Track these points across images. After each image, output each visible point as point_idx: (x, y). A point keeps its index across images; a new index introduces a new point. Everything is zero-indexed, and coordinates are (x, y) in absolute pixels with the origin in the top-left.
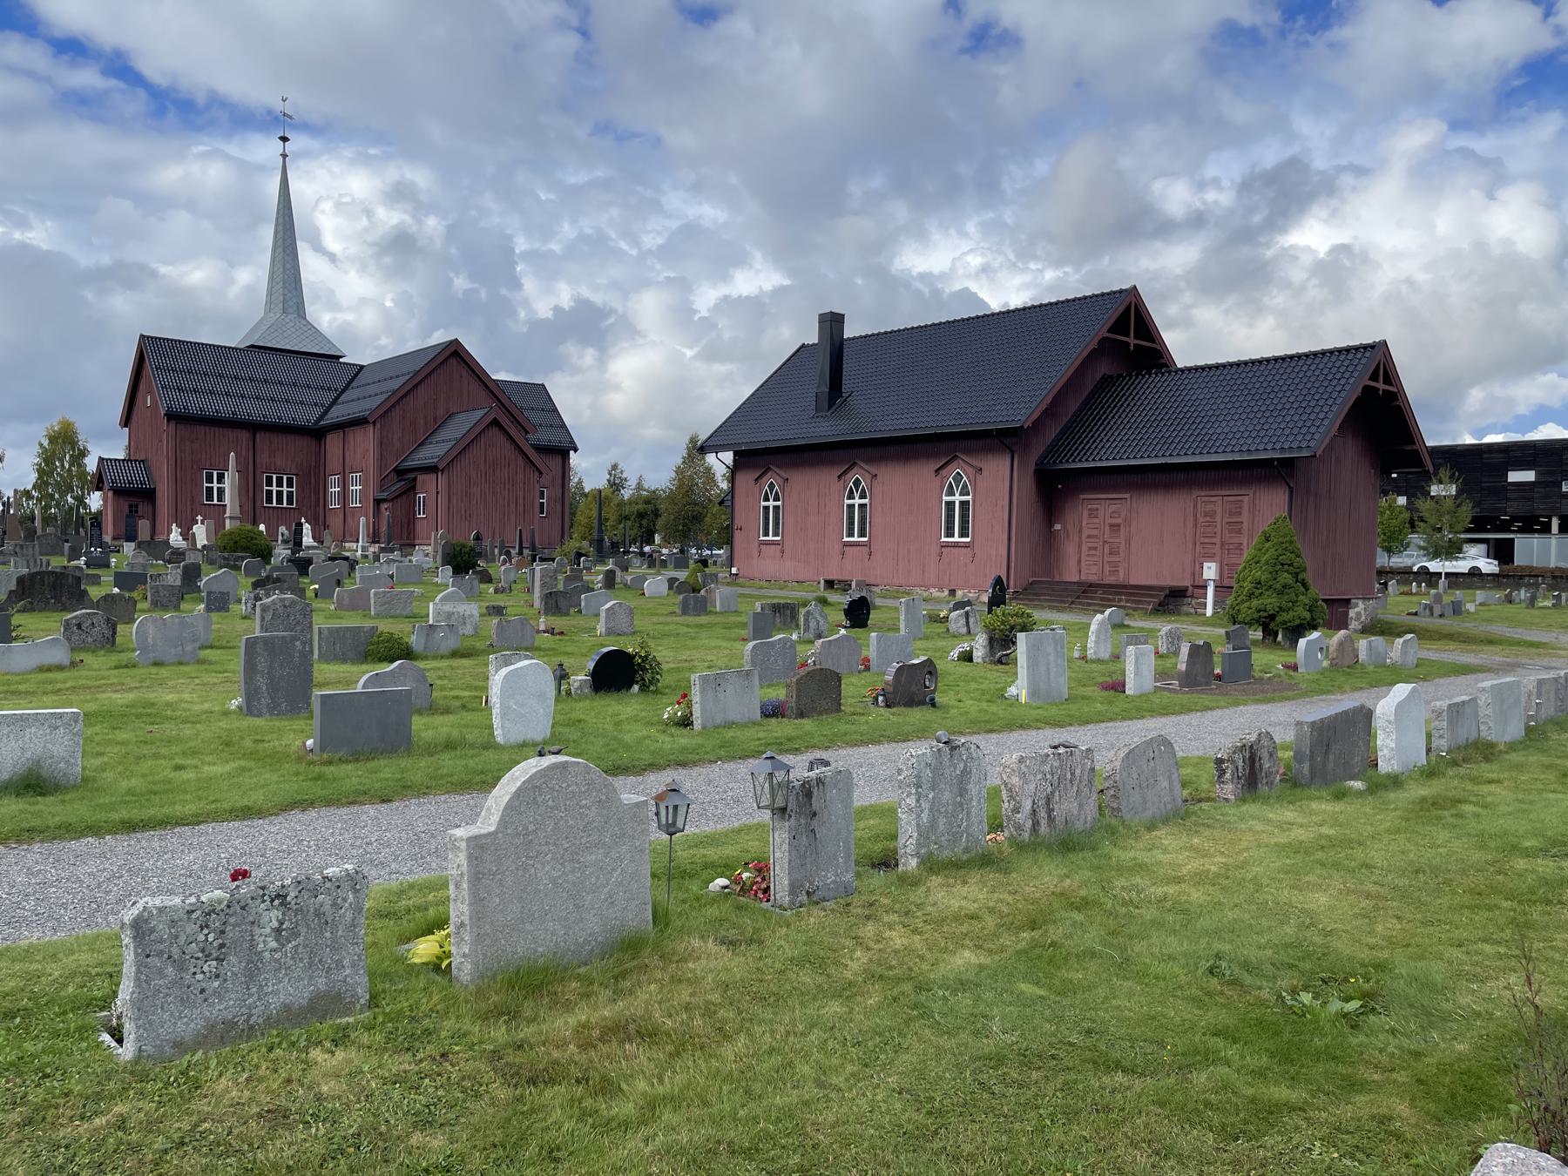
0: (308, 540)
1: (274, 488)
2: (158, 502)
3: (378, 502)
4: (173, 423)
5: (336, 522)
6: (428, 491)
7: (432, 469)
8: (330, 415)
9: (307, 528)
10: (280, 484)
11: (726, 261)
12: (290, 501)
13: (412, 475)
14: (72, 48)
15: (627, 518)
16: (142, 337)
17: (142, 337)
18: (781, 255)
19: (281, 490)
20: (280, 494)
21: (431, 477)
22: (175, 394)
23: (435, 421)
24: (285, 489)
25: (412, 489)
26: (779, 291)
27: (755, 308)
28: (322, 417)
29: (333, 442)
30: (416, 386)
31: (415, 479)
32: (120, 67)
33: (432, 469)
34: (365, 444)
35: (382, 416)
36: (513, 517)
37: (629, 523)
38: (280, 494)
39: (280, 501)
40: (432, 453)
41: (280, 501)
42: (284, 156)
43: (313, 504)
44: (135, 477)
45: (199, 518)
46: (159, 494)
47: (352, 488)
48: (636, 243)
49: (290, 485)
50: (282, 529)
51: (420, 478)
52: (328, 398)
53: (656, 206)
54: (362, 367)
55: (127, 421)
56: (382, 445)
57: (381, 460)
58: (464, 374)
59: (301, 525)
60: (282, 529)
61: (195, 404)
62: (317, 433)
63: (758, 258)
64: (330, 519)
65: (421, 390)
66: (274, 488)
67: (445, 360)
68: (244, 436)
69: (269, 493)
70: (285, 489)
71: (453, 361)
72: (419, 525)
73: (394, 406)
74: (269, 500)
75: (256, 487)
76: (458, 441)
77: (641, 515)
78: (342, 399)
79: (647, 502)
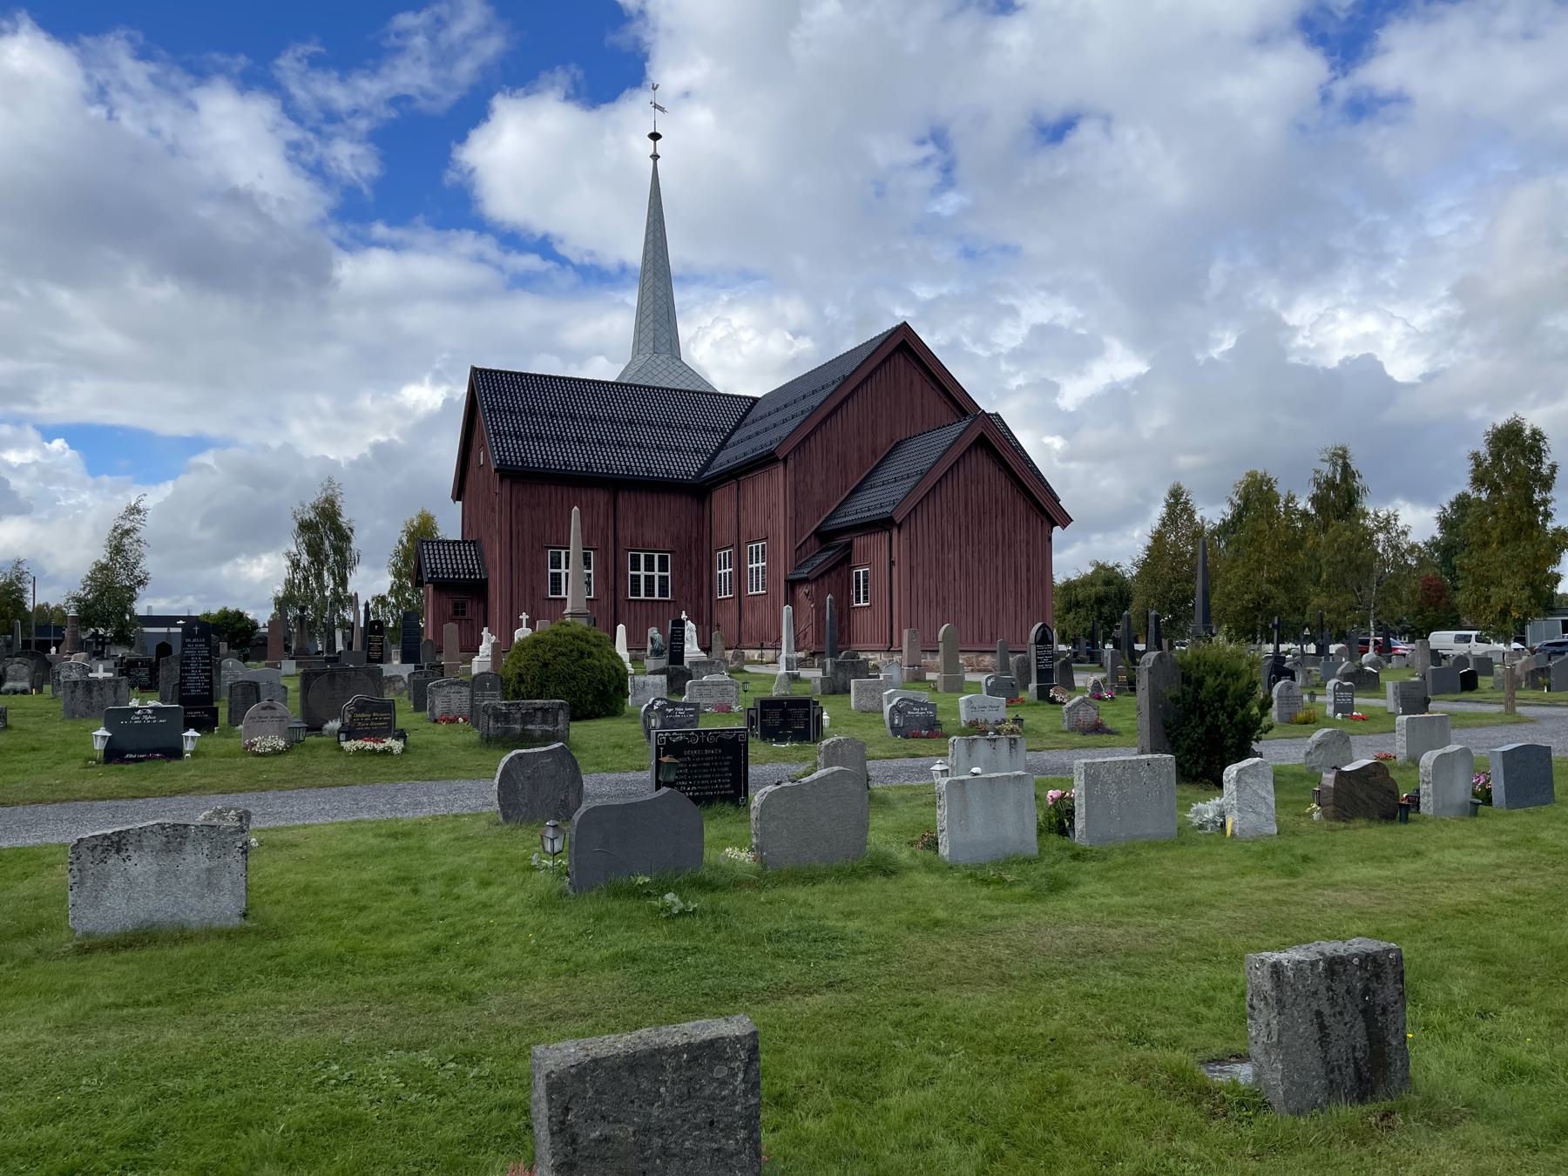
0: (692, 649)
1: (563, 570)
2: (491, 597)
3: (792, 585)
4: (507, 482)
5: (727, 617)
6: (872, 561)
7: (884, 524)
8: (715, 463)
9: (690, 626)
10: (649, 567)
11: (1081, 352)
12: (663, 592)
13: (845, 539)
14: (513, 239)
15: (1078, 604)
16: (474, 370)
17: (474, 370)
18: (1140, 341)
19: (650, 575)
20: (649, 579)
21: (877, 542)
22: (512, 443)
23: (874, 452)
24: (656, 573)
25: (845, 561)
26: (1138, 381)
27: (1118, 400)
28: (702, 471)
29: (722, 501)
30: (845, 400)
31: (850, 545)
32: (544, 247)
33: (884, 524)
34: (772, 491)
35: (797, 448)
36: (1011, 602)
37: (1083, 612)
38: (649, 579)
39: (650, 592)
40: (870, 504)
41: (650, 592)
42: (655, 157)
43: (695, 592)
44: (463, 566)
45: (524, 617)
46: (491, 586)
47: (755, 566)
48: (989, 345)
49: (663, 567)
50: (653, 632)
51: (860, 542)
52: (713, 442)
53: (1012, 311)
54: (756, 400)
55: (459, 494)
56: (798, 496)
57: (797, 517)
58: (917, 379)
59: (682, 623)
60: (653, 632)
61: (538, 455)
62: (698, 491)
63: (1116, 347)
64: (719, 616)
65: (852, 406)
66: (642, 573)
67: (888, 358)
68: (601, 498)
69: (636, 579)
70: (656, 573)
71: (900, 360)
72: (858, 619)
73: (813, 432)
74: (636, 592)
75: (618, 571)
76: (924, 474)
77: (1100, 601)
78: (734, 439)
79: (1108, 583)
